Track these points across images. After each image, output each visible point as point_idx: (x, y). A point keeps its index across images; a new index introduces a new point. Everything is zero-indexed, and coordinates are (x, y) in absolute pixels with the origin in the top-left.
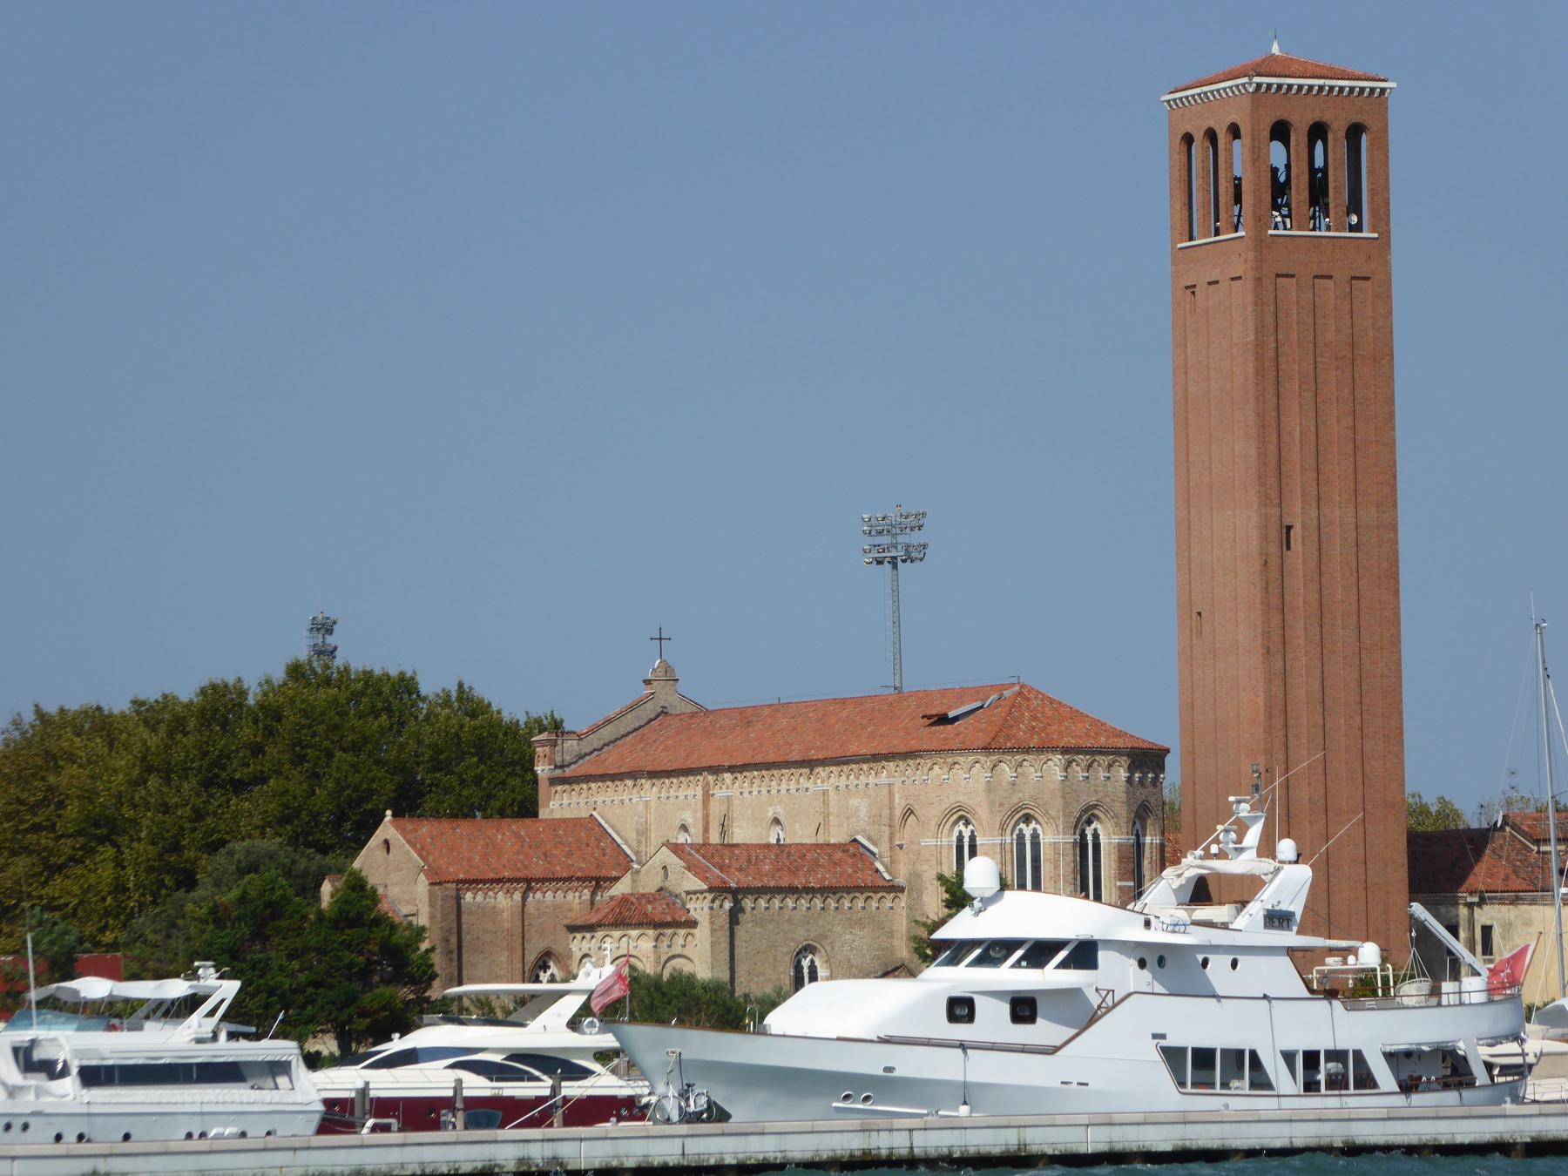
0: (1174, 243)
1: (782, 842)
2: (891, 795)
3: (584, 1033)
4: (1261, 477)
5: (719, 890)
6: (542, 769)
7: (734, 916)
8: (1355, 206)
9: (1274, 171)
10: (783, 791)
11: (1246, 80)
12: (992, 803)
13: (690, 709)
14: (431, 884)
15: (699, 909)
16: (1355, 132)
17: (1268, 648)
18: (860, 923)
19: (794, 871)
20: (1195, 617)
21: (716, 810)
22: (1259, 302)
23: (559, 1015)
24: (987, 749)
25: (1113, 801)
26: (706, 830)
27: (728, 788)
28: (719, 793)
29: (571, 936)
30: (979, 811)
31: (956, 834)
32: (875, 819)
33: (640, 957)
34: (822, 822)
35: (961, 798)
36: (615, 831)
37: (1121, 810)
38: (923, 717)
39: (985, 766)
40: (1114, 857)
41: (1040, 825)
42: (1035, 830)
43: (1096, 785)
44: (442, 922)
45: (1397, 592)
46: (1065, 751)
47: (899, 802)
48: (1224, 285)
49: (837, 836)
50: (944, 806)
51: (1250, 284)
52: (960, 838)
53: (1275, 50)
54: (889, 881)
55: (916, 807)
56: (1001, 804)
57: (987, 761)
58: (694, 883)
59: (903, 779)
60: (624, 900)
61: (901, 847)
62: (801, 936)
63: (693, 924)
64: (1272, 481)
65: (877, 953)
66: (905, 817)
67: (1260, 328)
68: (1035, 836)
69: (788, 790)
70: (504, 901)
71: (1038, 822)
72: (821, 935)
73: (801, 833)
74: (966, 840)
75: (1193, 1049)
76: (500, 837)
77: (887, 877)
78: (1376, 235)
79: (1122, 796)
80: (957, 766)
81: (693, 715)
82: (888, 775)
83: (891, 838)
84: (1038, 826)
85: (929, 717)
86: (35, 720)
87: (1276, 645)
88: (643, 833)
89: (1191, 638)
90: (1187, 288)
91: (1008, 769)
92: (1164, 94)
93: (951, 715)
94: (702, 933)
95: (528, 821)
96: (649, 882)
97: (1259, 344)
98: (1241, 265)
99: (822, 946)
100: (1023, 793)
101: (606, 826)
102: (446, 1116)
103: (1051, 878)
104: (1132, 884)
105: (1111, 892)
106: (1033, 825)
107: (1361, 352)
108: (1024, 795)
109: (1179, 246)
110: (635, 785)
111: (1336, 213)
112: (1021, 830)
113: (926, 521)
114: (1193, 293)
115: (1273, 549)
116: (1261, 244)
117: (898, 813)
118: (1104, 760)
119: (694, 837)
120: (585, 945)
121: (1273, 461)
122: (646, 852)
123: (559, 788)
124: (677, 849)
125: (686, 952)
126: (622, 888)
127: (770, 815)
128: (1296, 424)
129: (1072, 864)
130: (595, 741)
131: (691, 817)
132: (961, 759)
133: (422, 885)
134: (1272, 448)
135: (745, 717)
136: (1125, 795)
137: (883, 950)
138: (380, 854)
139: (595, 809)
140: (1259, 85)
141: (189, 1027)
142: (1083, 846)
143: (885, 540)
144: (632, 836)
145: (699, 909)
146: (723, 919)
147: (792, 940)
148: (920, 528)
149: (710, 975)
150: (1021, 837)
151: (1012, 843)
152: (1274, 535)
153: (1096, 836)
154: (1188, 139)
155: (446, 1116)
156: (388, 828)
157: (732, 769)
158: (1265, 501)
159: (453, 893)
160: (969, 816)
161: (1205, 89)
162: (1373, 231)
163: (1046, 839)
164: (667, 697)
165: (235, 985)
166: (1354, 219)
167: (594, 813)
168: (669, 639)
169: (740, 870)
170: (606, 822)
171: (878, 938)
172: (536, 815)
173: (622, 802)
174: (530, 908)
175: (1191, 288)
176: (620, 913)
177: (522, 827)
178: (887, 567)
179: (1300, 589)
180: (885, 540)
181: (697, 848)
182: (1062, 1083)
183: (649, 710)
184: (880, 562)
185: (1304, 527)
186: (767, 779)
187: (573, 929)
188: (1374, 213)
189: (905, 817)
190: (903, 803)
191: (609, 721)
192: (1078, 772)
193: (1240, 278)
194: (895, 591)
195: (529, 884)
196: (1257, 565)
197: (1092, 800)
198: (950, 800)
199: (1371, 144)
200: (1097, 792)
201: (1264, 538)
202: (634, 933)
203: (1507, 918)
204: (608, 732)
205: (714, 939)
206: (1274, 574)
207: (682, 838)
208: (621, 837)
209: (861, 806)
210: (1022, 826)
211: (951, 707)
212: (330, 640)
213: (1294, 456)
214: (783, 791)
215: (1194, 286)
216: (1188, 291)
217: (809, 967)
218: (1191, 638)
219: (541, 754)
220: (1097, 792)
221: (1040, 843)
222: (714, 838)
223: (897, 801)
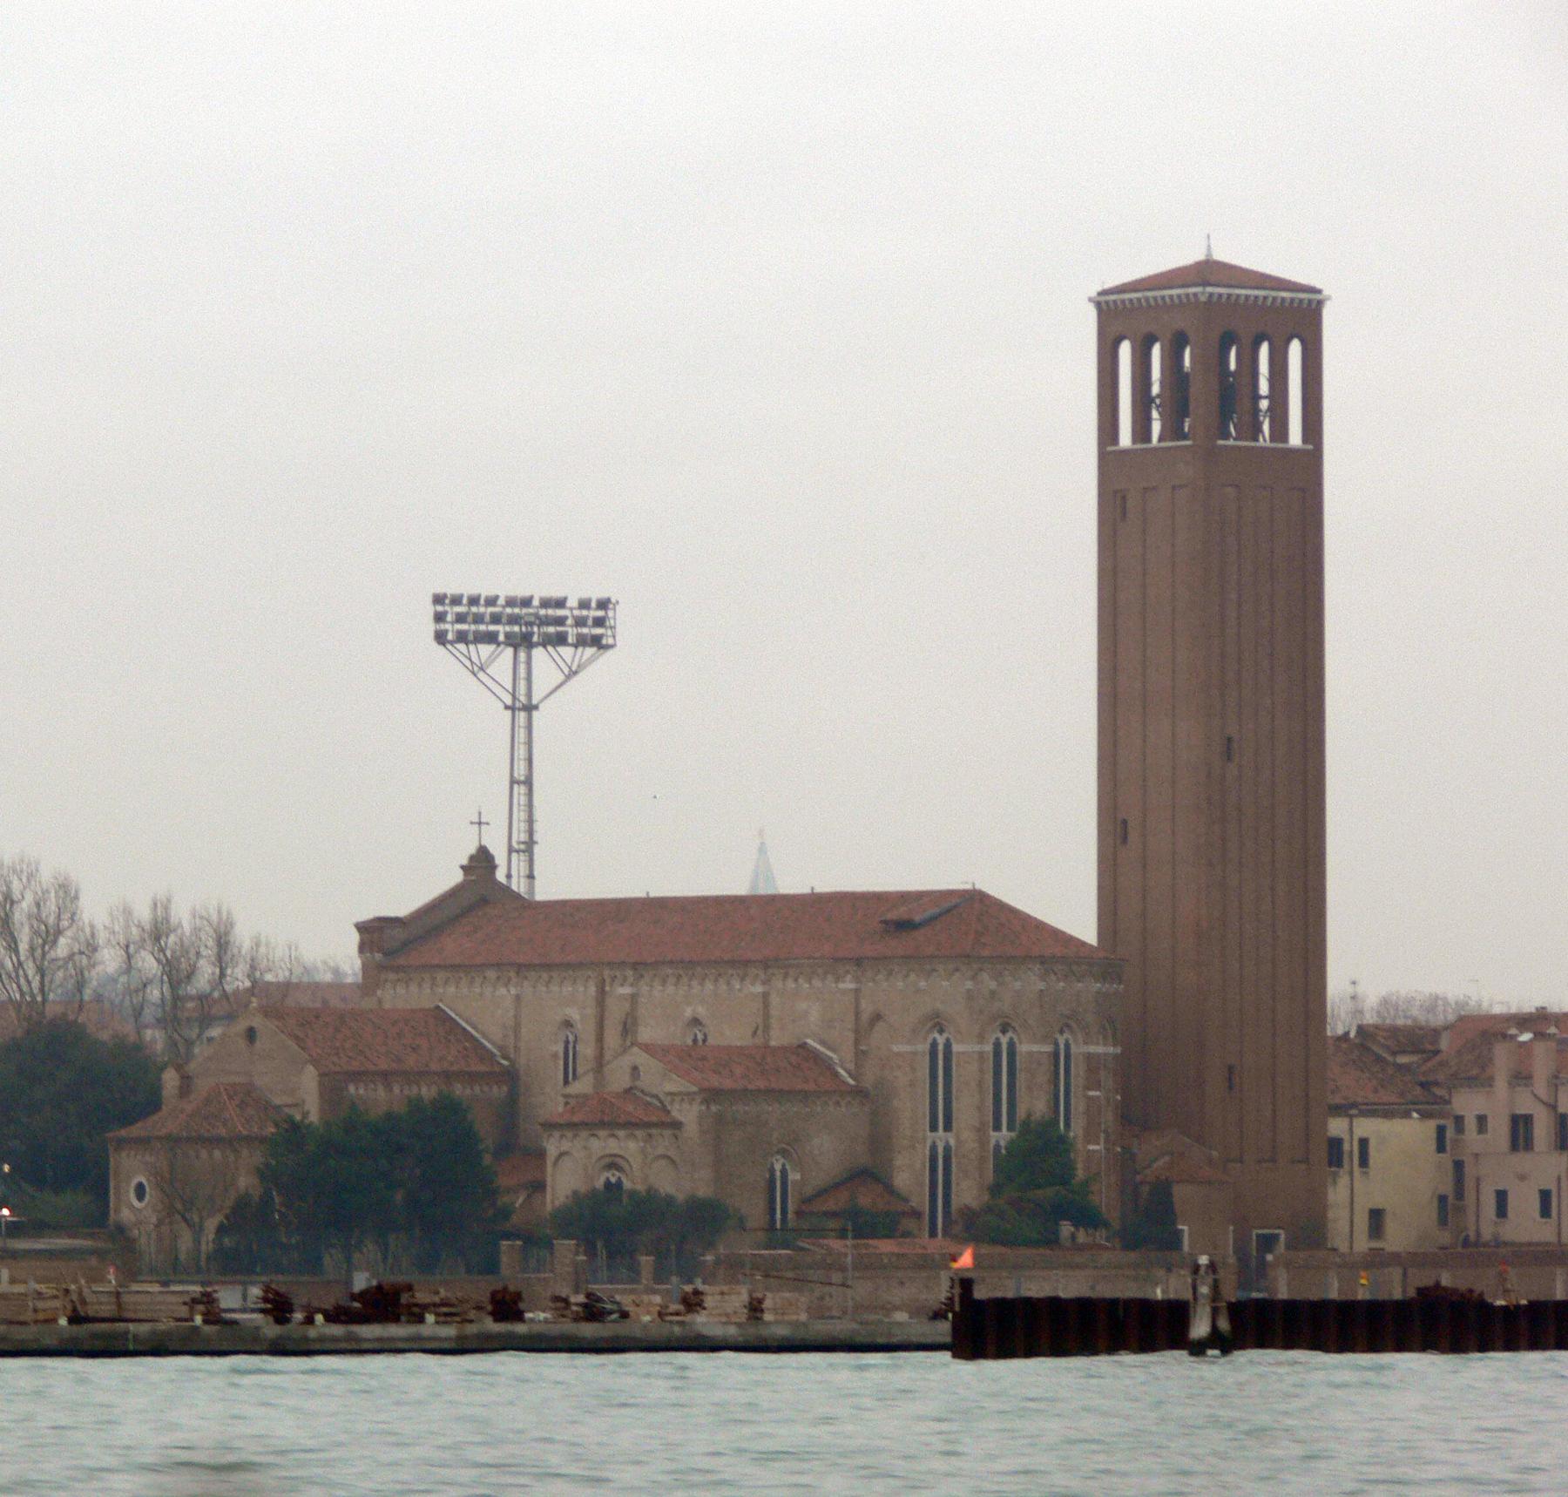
21: (616, 1012)
31: (930, 1040)
33: (627, 1157)
35: (939, 1005)
41: (1018, 1035)
42: (1011, 1039)
47: (867, 1008)
52: (934, 1045)
56: (981, 1012)
58: (674, 1084)
63: (677, 1125)
68: (1011, 1045)
74: (941, 1048)
77: (851, 1082)
80: (935, 974)
86: (139, 926)
93: (917, 918)
102: (908, 1224)
110: (498, 978)
120: (566, 1145)
127: (688, 1013)
140: (1211, 295)
150: (934, 1045)
155: (908, 1224)
163: (1023, 1048)
167: (441, 1005)
170: (457, 1015)
186: (685, 979)
203: (255, 1299)
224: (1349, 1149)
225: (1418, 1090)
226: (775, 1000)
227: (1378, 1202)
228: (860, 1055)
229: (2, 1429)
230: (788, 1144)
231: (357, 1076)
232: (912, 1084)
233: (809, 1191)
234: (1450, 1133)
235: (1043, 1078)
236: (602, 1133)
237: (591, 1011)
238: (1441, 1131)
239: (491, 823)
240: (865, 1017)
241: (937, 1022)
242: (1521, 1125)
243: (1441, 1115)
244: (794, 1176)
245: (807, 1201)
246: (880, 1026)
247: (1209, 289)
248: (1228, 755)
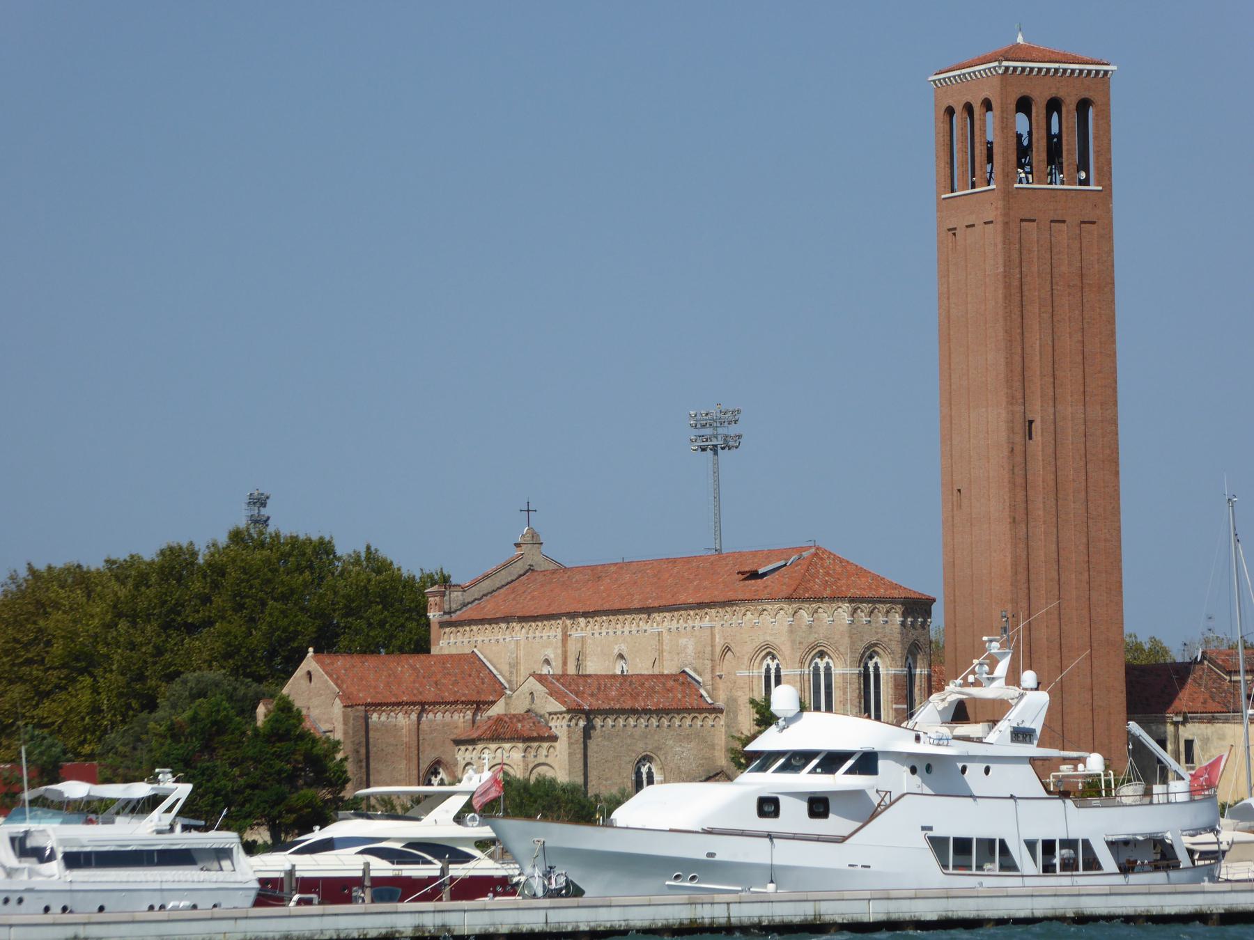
0: (939, 194)
1: (625, 673)
2: (713, 636)
3: (467, 826)
4: (1009, 381)
5: (575, 712)
6: (433, 615)
7: (587, 732)
8: (1083, 164)
9: (1019, 136)
10: (626, 633)
11: (996, 64)
12: (793, 642)
13: (552, 566)
14: (345, 707)
15: (559, 726)
16: (1083, 106)
17: (1014, 518)
18: (688, 738)
19: (635, 696)
20: (956, 494)
21: (573, 648)
22: (1007, 242)
23: (447, 812)
24: (789, 599)
25: (890, 640)
26: (565, 663)
27: (582, 630)
28: (575, 634)
29: (457, 748)
30: (783, 648)
31: (764, 666)
32: (699, 654)
34: (658, 657)
36: (492, 664)
37: (897, 647)
38: (738, 573)
39: (788, 612)
40: (891, 685)
41: (832, 659)
42: (828, 663)
43: (876, 628)
44: (353, 737)
45: (1117, 473)
46: (852, 600)
47: (719, 641)
48: (978, 229)
49: (669, 668)
50: (755, 644)
51: (999, 227)
52: (768, 670)
53: (1020, 40)
54: (711, 704)
55: (733, 645)
56: (801, 643)
57: (789, 608)
58: (555, 706)
59: (722, 622)
60: (499, 720)
61: (720, 677)
62: (640, 748)
63: (554, 738)
64: (1017, 385)
65: (701, 762)
66: (724, 653)
67: (1008, 262)
68: (828, 668)
69: (630, 632)
70: (403, 720)
71: (830, 657)
72: (656, 747)
73: (640, 666)
74: (773, 671)
75: (954, 839)
76: (400, 669)
77: (710, 701)
78: (1100, 188)
79: (898, 636)
80: (765, 612)
81: (554, 572)
82: (710, 619)
83: (713, 670)
84: (830, 661)
85: (743, 573)
87: (1021, 516)
88: (514, 665)
89: (953, 510)
90: (949, 230)
91: (806, 615)
92: (931, 75)
94: (561, 746)
95: (422, 657)
96: (519, 705)
97: (1007, 275)
98: (992, 212)
99: (657, 756)
100: (818, 634)
101: (485, 660)
102: (357, 892)
103: (840, 702)
104: (905, 706)
105: (888, 713)
106: (826, 659)
107: (1088, 282)
109: (943, 196)
110: (507, 628)
111: (1068, 170)
112: (816, 664)
113: (741, 417)
114: (954, 234)
115: (1018, 438)
116: (1008, 195)
117: (718, 650)
118: (883, 607)
119: (555, 669)
120: (468, 756)
121: (1018, 368)
122: (517, 681)
123: (447, 630)
124: (541, 679)
125: (548, 761)
126: (497, 710)
127: (616, 651)
128: (1036, 339)
129: (858, 691)
130: (475, 592)
131: (553, 653)
132: (769, 607)
134: (1018, 358)
135: (596, 573)
136: (899, 636)
137: (706, 759)
138: (304, 682)
139: (476, 647)
140: (1007, 68)
142: (866, 676)
143: (707, 432)
145: (559, 726)
146: (579, 735)
147: (634, 751)
148: (736, 422)
149: (567, 779)
150: (817, 669)
151: (809, 674)
152: (1019, 427)
153: (876, 668)
154: (950, 111)
155: (357, 892)
156: (310, 662)
157: (585, 615)
158: (1011, 401)
159: (363, 714)
160: (775, 652)
161: (964, 71)
162: (1098, 185)
163: (837, 671)
164: (533, 557)
165: (188, 788)
166: (1083, 175)
167: (475, 650)
168: (535, 511)
169: (592, 695)
170: (485, 657)
171: (702, 749)
172: (428, 651)
173: (498, 641)
175: (953, 230)
176: (496, 730)
177: (418, 661)
178: (709, 453)
179: (1039, 470)
181: (558, 678)
182: (849, 865)
183: (519, 568)
184: (704, 450)
185: (1043, 421)
186: (613, 623)
187: (458, 742)
188: (1098, 169)
189: (724, 653)
190: (722, 642)
191: (487, 577)
192: (863, 617)
193: (992, 222)
194: (716, 472)
196: (1005, 452)
197: (873, 640)
198: (759, 640)
199: (1096, 116)
200: (877, 633)
201: (1011, 430)
202: (507, 746)
204: (486, 586)
205: (571, 751)
206: (1019, 459)
207: (545, 670)
208: (497, 669)
209: (689, 644)
210: (818, 660)
211: (760, 566)
212: (264, 511)
214: (626, 633)
215: (955, 229)
216: (950, 233)
217: (647, 773)
218: (953, 510)
219: (433, 603)
220: (877, 633)
221: (831, 674)
222: (571, 670)
223: (717, 640)
224: (392, 871)
226: (666, 635)
230: (645, 752)
231: (377, 706)
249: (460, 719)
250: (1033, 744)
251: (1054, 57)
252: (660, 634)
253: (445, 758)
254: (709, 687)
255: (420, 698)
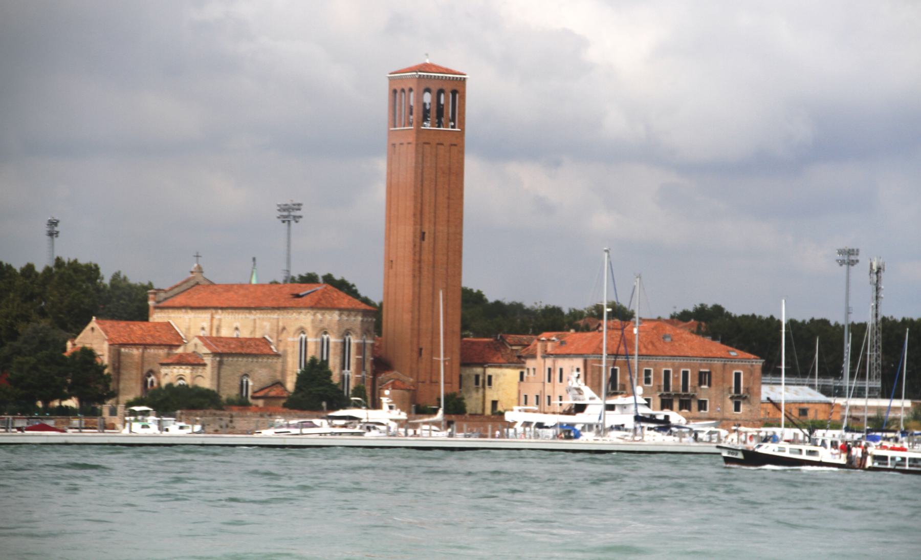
0: (389, 128)
2: (278, 322)
5: (215, 354)
6: (151, 303)
7: (221, 363)
8: (453, 120)
9: (425, 104)
13: (207, 283)
14: (110, 345)
15: (208, 360)
16: (454, 92)
18: (265, 367)
19: (242, 347)
20: (390, 264)
21: (215, 323)
24: (312, 308)
26: (211, 329)
27: (219, 315)
28: (217, 317)
32: (272, 329)
37: (358, 330)
46: (340, 310)
47: (281, 324)
49: (258, 335)
51: (414, 146)
52: (301, 339)
57: (312, 312)
58: (206, 350)
60: (181, 355)
62: (243, 370)
63: (205, 365)
64: (418, 216)
67: (417, 162)
70: (136, 352)
73: (245, 334)
78: (459, 130)
79: (359, 326)
81: (208, 286)
82: (275, 316)
87: (417, 272)
88: (188, 329)
93: (301, 294)
94: (209, 369)
95: (145, 323)
96: (190, 349)
97: (416, 167)
98: (411, 138)
108: (325, 325)
115: (418, 240)
116: (419, 132)
118: (353, 313)
119: (206, 333)
124: (200, 338)
126: (180, 350)
130: (170, 293)
131: (206, 325)
133: (106, 345)
135: (228, 288)
138: (90, 333)
140: (420, 75)
141: (664, 440)
143: (285, 213)
144: (184, 330)
145: (208, 360)
146: (216, 364)
150: (301, 339)
152: (418, 234)
153: (349, 340)
154: (395, 91)
156: (94, 323)
157: (222, 308)
158: (415, 223)
162: (459, 128)
163: (309, 340)
164: (199, 278)
166: (452, 124)
169: (223, 346)
172: (147, 320)
174: (146, 355)
175: (394, 145)
177: (142, 325)
178: (286, 223)
180: (285, 213)
181: (207, 338)
183: (192, 283)
184: (284, 222)
185: (429, 233)
187: (162, 364)
188: (459, 121)
191: (176, 286)
194: (289, 234)
195: (146, 346)
196: (412, 246)
197: (348, 327)
199: (460, 97)
201: (415, 236)
202: (184, 367)
204: (176, 290)
206: (418, 249)
207: (202, 334)
209: (267, 325)
212: (56, 229)
213: (426, 209)
222: (214, 335)
225: (516, 358)
226: (258, 321)
227: (495, 398)
228: (279, 341)
229: (0, 469)
232: (293, 352)
233: (256, 389)
234: (525, 374)
235: (339, 350)
236: (178, 367)
237: (209, 324)
238: (522, 374)
239: (253, 256)
240: (280, 328)
241: (302, 331)
242: (704, 375)
243: (523, 368)
244: (250, 383)
245: (255, 392)
246: (285, 332)
247: (419, 73)
248: (423, 238)
249: (162, 352)
250: (125, 410)
251: (442, 70)
252: (255, 320)
253: (155, 369)
254: (275, 345)
255: (144, 342)
